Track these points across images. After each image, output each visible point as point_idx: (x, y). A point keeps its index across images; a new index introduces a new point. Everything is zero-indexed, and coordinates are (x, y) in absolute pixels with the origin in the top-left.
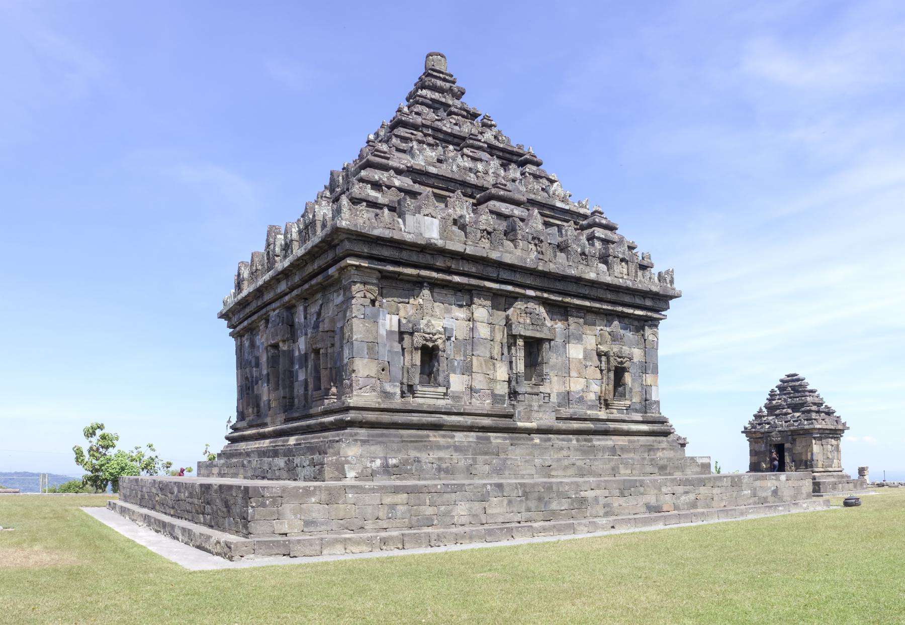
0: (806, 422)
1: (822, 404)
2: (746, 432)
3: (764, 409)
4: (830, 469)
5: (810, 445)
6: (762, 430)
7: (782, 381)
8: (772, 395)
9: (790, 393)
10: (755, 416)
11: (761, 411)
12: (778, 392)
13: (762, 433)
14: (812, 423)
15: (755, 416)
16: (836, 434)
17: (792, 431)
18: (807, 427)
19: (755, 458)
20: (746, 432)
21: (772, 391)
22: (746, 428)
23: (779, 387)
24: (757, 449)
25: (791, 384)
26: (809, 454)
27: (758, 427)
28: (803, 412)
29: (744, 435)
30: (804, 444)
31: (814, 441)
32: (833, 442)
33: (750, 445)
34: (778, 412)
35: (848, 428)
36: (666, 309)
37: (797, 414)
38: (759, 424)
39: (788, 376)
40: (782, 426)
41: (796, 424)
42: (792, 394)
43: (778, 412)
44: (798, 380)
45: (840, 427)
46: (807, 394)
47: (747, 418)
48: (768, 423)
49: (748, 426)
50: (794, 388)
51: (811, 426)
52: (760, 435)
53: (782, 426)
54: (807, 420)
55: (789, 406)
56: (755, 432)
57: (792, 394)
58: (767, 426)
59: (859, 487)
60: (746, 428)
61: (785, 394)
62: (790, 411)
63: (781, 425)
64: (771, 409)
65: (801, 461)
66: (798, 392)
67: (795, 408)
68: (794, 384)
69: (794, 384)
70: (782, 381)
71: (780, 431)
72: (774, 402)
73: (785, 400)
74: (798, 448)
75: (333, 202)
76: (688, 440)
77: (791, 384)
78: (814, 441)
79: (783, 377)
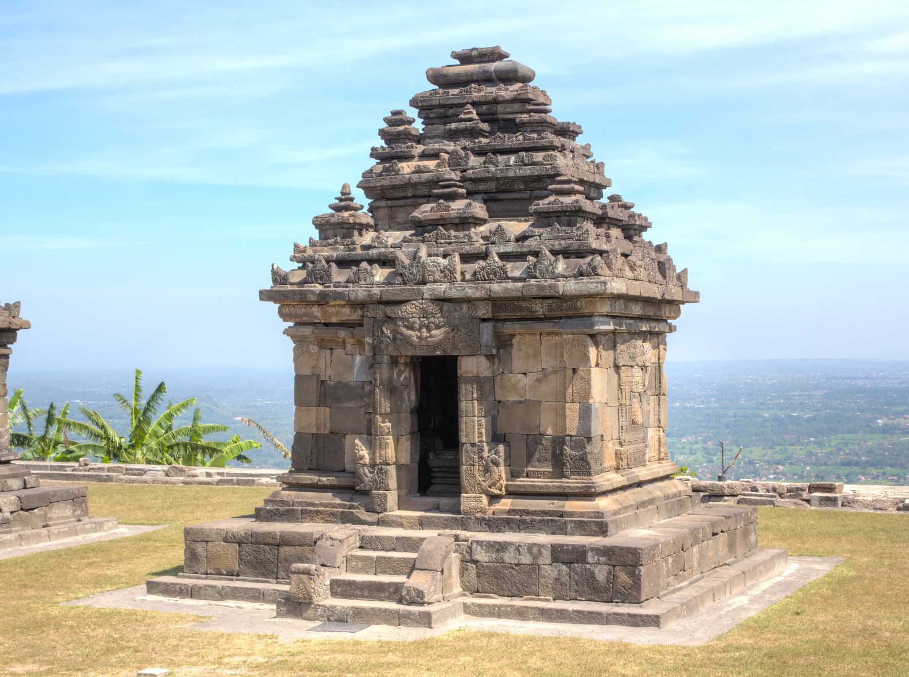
0: (561, 266)
1: (599, 187)
2: (281, 294)
3: (361, 199)
4: (643, 473)
5: (574, 371)
6: (359, 292)
7: (436, 77)
8: (395, 134)
9: (473, 133)
10: (322, 224)
11: (344, 203)
12: (418, 126)
13: (361, 305)
14: (593, 272)
15: (322, 224)
16: (652, 315)
17: (497, 302)
18: (570, 286)
19: (320, 418)
20: (281, 294)
21: (396, 119)
22: (279, 277)
23: (422, 104)
24: (329, 373)
25: (478, 93)
26: (572, 411)
27: (339, 276)
28: (545, 218)
29: (273, 307)
30: (548, 362)
31: (593, 352)
32: (646, 350)
33: (299, 355)
34: (426, 211)
35: (695, 297)
36: (12, 343)
37: (515, 227)
38: (343, 263)
39: (465, 58)
40: (448, 274)
41: (516, 269)
42: (483, 137)
43: (426, 211)
44: (511, 76)
45: (674, 293)
46: (551, 137)
47: (284, 236)
48: (384, 262)
49: (288, 266)
50: (489, 111)
51: (587, 285)
52: (346, 314)
53: (448, 274)
54: (566, 253)
55: (475, 188)
56: (323, 300)
57: (483, 137)
58: (380, 274)
59: (740, 550)
60: (279, 277)
61: (452, 136)
62: (479, 209)
63: (443, 269)
64: (391, 196)
65: (533, 440)
66: (512, 126)
67: (503, 197)
68: (490, 91)
69: (490, 91)
70: (436, 77)
71: (440, 300)
72: (406, 168)
73: (455, 161)
74: (523, 378)
75: (435, 476)
76: (24, 314)
77: (478, 93)
78: (593, 352)
79: (445, 61)
